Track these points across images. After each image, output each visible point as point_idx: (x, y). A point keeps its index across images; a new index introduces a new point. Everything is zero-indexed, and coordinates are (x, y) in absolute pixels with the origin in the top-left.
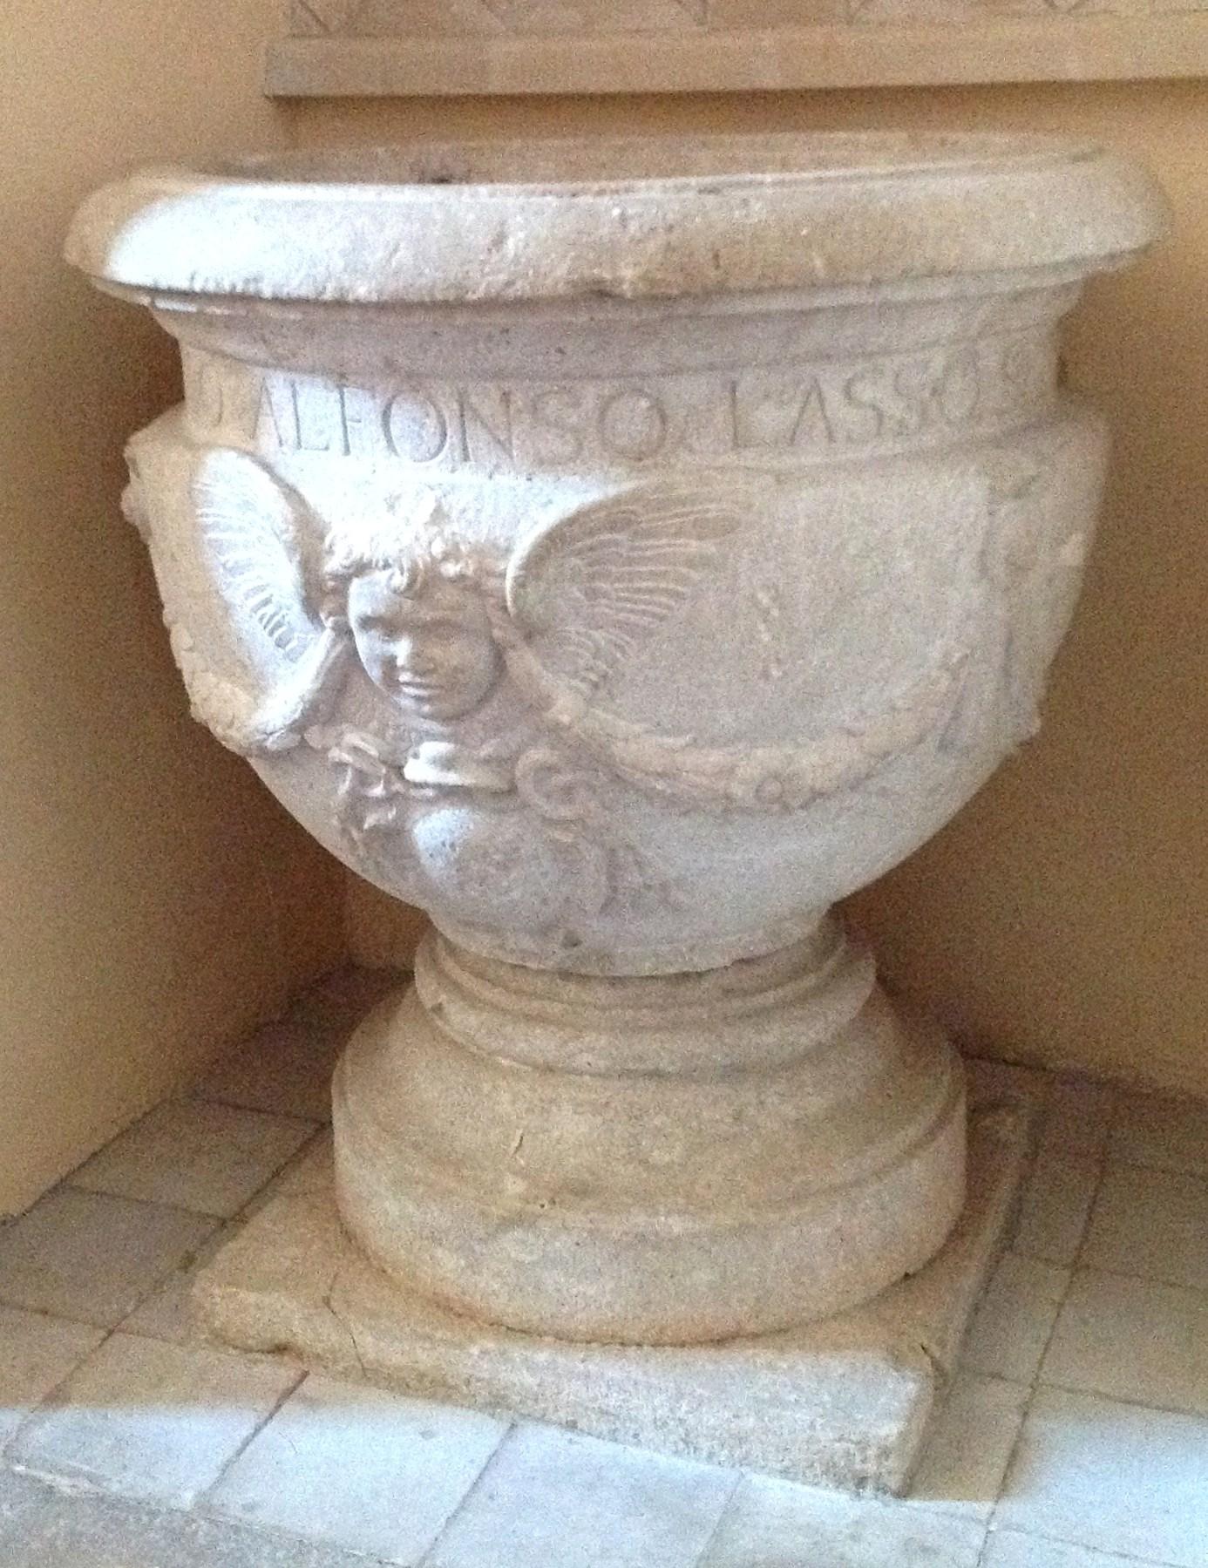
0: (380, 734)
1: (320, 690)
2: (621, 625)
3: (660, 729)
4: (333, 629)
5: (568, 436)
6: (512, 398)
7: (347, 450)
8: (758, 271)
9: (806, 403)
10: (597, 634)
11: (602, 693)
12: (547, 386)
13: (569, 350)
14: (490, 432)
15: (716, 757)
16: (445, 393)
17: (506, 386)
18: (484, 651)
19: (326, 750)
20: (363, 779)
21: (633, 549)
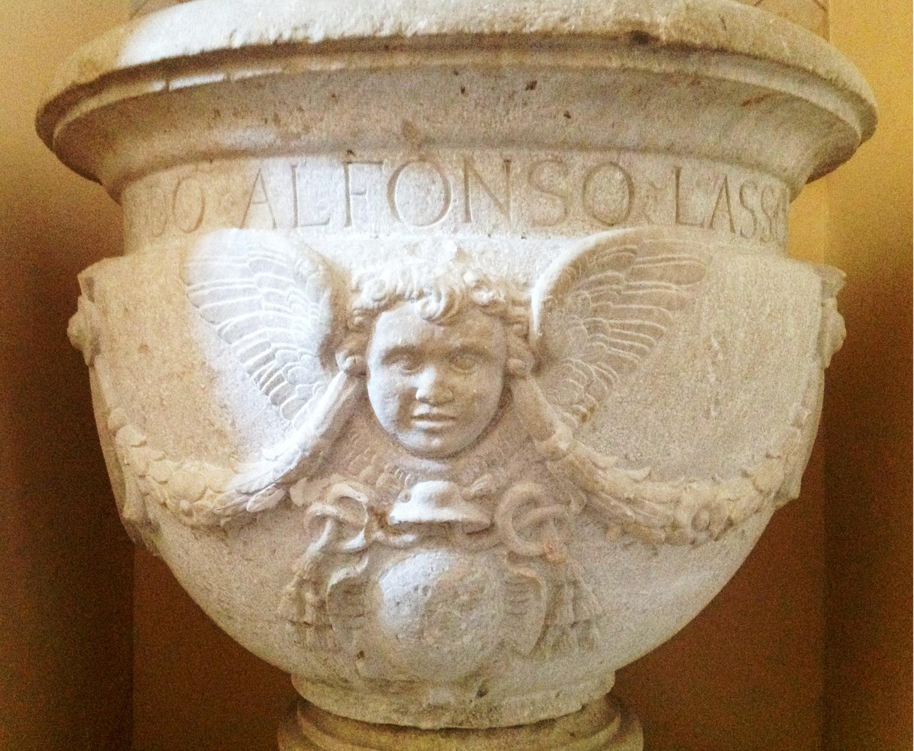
0: (370, 482)
1: (323, 436)
2: (610, 359)
3: (628, 462)
4: (347, 371)
5: (559, 202)
6: (512, 165)
7: (348, 221)
8: (751, 39)
9: (720, 197)
10: (592, 368)
11: (587, 426)
12: (542, 155)
13: (574, 115)
14: (491, 195)
15: (665, 490)
16: (451, 157)
17: (508, 152)
18: (498, 382)
19: (305, 506)
20: (342, 528)
21: (630, 287)
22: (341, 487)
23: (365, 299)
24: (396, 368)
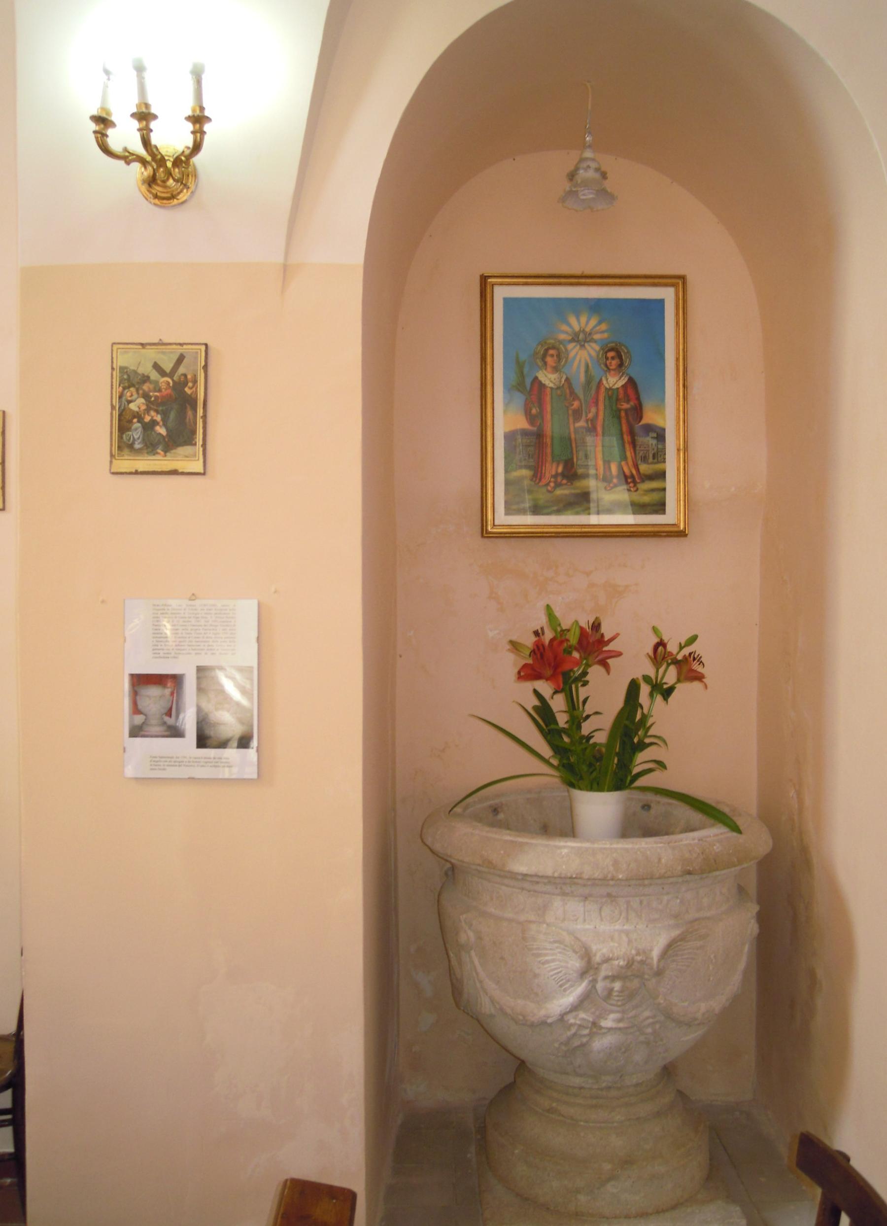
17: (642, 898)
22: (582, 1015)
23: (598, 959)
24: (608, 981)
